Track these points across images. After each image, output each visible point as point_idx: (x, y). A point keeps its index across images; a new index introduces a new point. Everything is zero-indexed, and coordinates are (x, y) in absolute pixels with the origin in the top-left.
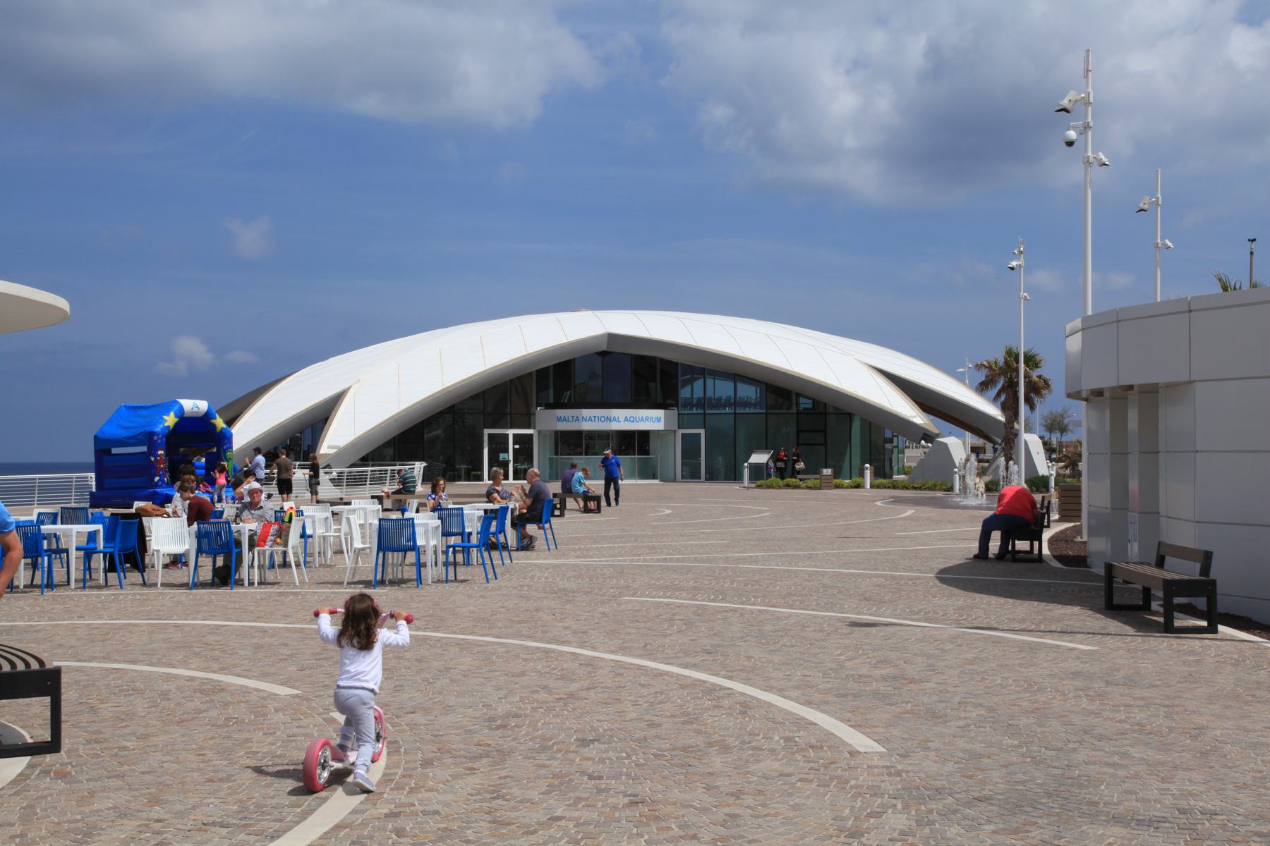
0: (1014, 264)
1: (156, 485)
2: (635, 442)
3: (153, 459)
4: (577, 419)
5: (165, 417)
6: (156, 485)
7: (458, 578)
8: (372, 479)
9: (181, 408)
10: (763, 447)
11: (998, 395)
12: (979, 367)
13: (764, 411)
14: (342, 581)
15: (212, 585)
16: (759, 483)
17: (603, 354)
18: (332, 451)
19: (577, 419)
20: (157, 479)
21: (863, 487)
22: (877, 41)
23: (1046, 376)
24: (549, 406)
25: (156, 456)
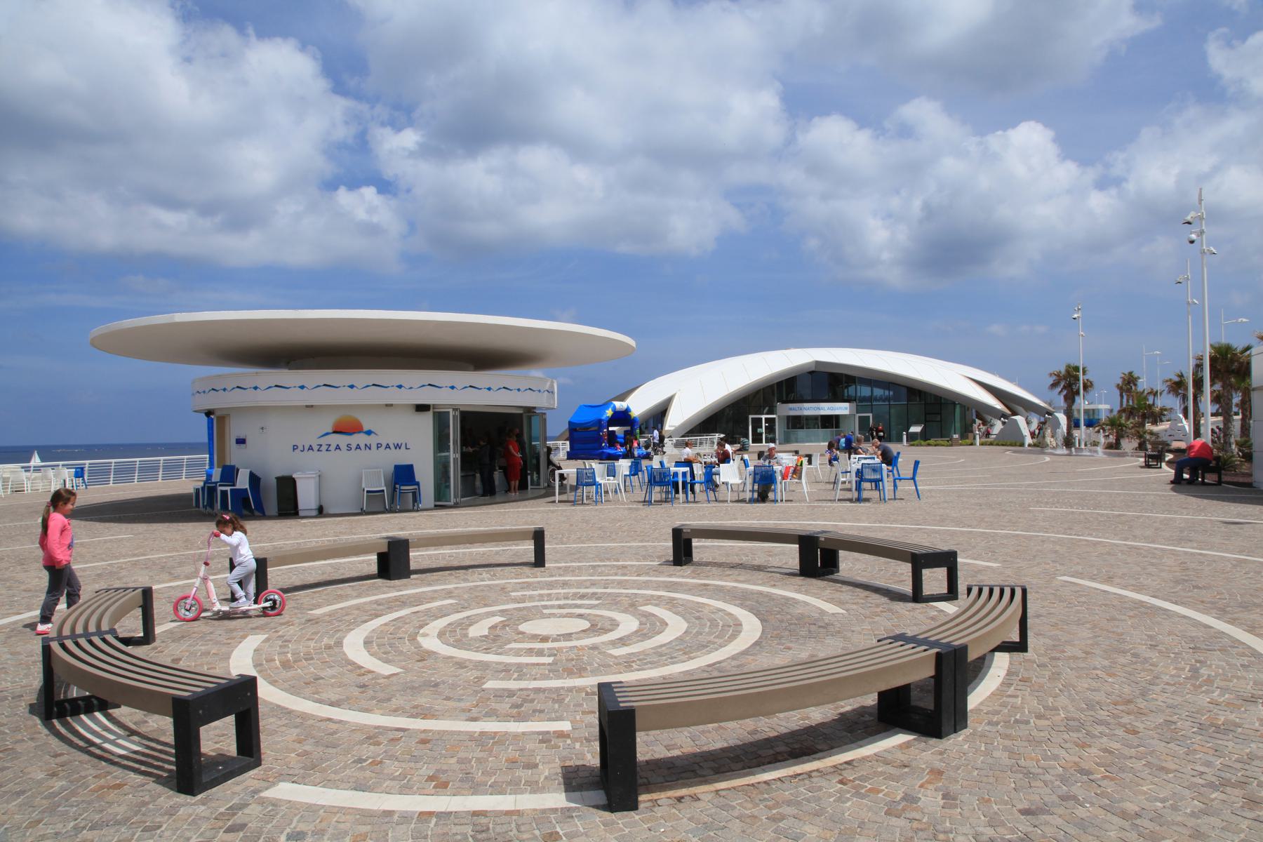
0: (1076, 316)
1: (603, 448)
2: (830, 422)
4: (801, 409)
5: (607, 411)
6: (603, 448)
7: (896, 497)
9: (615, 406)
10: (917, 423)
12: (1051, 375)
13: (906, 403)
15: (752, 501)
16: (912, 443)
17: (811, 373)
18: (672, 428)
19: (801, 409)
20: (603, 444)
22: (895, 203)
23: (1091, 379)
25: (603, 432)
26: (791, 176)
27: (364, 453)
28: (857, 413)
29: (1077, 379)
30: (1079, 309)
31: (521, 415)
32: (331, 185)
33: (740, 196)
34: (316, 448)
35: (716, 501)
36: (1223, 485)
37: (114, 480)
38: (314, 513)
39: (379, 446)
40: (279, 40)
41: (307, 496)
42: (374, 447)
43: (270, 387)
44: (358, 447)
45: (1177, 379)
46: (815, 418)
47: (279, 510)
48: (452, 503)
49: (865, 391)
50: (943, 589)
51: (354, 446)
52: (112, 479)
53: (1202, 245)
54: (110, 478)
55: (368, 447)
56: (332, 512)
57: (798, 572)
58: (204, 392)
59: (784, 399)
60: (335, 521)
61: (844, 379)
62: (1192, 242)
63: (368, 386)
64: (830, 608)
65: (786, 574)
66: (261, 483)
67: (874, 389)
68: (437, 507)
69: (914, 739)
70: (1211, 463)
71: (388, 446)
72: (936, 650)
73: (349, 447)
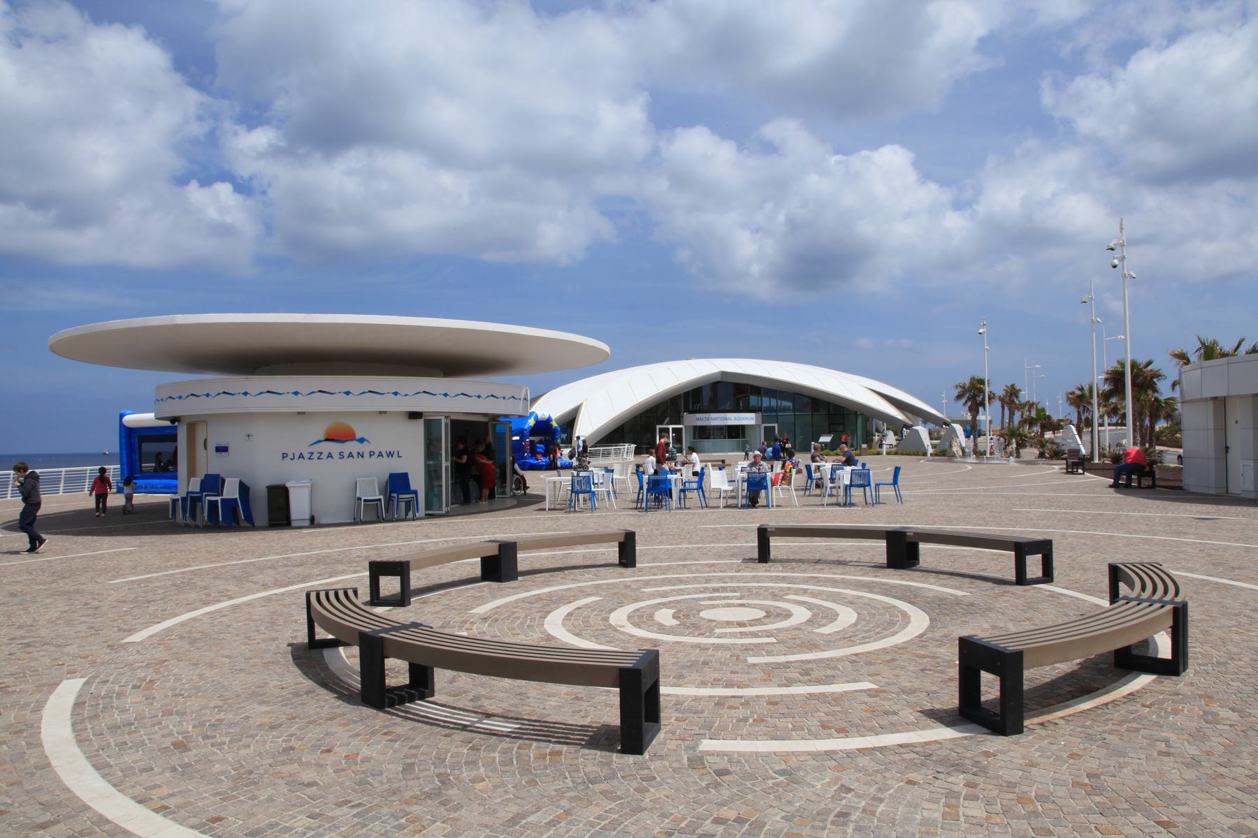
0: (981, 331)
1: (525, 458)
2: (735, 432)
3: (524, 443)
4: (708, 419)
5: (529, 421)
6: (525, 458)
8: (603, 454)
11: (966, 403)
14: (829, 498)
15: (743, 507)
19: (708, 419)
20: (526, 454)
21: (882, 454)
24: (690, 412)
25: (525, 442)
26: (657, 187)
27: (357, 461)
28: (763, 423)
29: (982, 391)
30: (984, 324)
31: (486, 424)
32: (181, 181)
33: (612, 208)
34: (307, 456)
35: (707, 507)
36: (1157, 488)
37: (12, 494)
38: (307, 523)
39: (371, 454)
40: (117, 27)
41: (299, 506)
42: (367, 455)
43: (313, 392)
44: (351, 455)
45: (1078, 393)
46: (721, 428)
47: (270, 521)
48: (444, 512)
49: (766, 402)
50: (1039, 574)
51: (346, 455)
52: (10, 492)
53: (1123, 270)
54: (59, 487)
55: (361, 455)
56: (324, 521)
57: (886, 565)
58: (504, 398)
59: (691, 409)
60: (348, 530)
61: (749, 389)
62: (1115, 267)
63: (262, 393)
64: (959, 593)
65: (871, 567)
66: (250, 492)
67: (771, 400)
68: (429, 516)
69: (1154, 681)
70: (1145, 468)
71: (380, 455)
72: (1172, 606)
73: (341, 455)
